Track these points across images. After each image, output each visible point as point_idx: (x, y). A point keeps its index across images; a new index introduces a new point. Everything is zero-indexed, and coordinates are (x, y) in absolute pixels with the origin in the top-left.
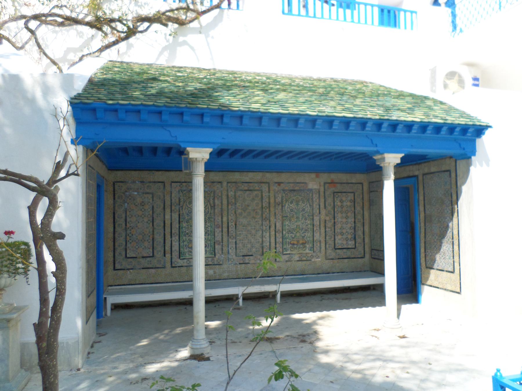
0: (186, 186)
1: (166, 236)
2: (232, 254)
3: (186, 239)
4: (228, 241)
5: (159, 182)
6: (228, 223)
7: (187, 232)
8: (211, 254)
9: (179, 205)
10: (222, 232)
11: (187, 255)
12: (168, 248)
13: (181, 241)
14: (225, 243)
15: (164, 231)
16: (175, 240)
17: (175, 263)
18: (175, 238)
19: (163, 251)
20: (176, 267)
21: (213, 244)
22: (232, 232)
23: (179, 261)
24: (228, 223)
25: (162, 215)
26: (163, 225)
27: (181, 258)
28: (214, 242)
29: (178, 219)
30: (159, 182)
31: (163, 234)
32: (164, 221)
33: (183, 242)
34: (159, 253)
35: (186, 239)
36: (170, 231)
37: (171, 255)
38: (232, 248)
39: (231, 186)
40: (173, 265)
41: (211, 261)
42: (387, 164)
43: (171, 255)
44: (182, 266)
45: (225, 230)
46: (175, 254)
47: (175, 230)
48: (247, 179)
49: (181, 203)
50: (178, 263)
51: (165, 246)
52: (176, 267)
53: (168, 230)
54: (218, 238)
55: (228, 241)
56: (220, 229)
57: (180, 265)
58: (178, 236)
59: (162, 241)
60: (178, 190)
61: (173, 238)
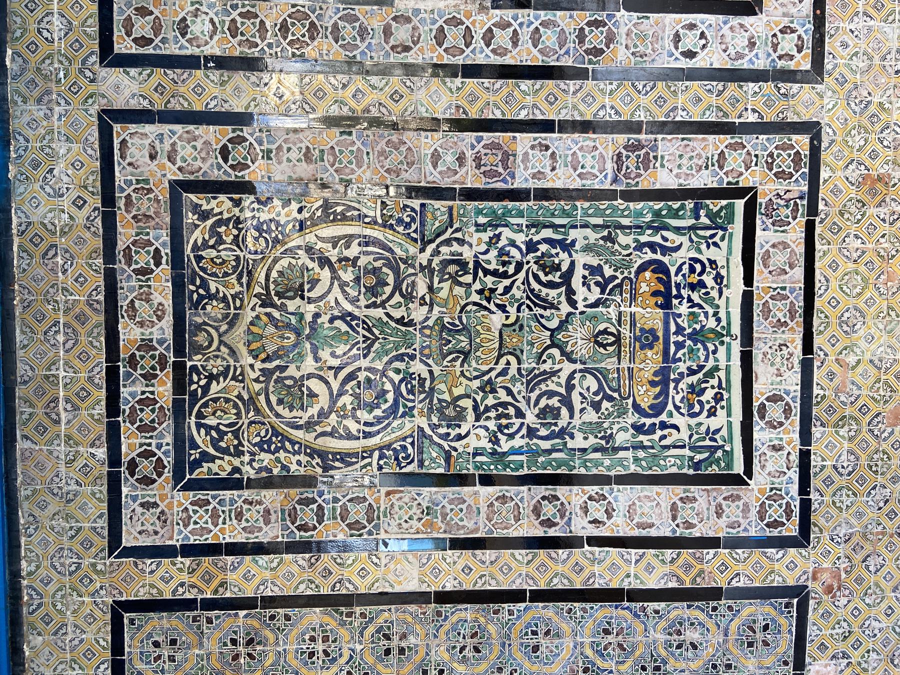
0: (147, 402)
1: (559, 584)
2: (741, 42)
3: (589, 429)
4: (624, 75)
5: (117, 646)
6: (472, 71)
7: (531, 418)
8: (719, 223)
9: (308, 482)
10: (547, 126)
11: (714, 423)
12: (653, 571)
13: (605, 465)
14: (643, 106)
15: (516, 596)
16: (597, 511)
17: (775, 512)
18: (578, 512)
19: (679, 610)
20: (806, 507)
21: (646, 209)
22: (549, 38)
23: (760, 481)
24: (472, 71)
25: (388, 614)
26: (468, 612)
27: (739, 468)
28: (629, 196)
29: (428, 492)
30: (117, 646)
31: (547, 611)
32: (443, 597)
33: (608, 447)
34: (692, 635)
35: (589, 429)
36: (521, 554)
37: (712, 543)
38: (690, 41)
39: (142, 27)
40: (792, 529)
41: (781, 223)
42: (18, 113)
43: (712, 543)
44: (805, 457)
45: (528, 99)
46: (705, 511)
47: (519, 512)
48: (77, 280)
49: (296, 465)
50: (775, 495)
51: (636, 595)
52: (806, 507)
53: (516, 570)
54: (587, 162)
55: (624, 75)
56: (524, 141)
57: (794, 475)
58: (561, 491)
59: (602, 611)
60: (184, 499)
61: (581, 527)
